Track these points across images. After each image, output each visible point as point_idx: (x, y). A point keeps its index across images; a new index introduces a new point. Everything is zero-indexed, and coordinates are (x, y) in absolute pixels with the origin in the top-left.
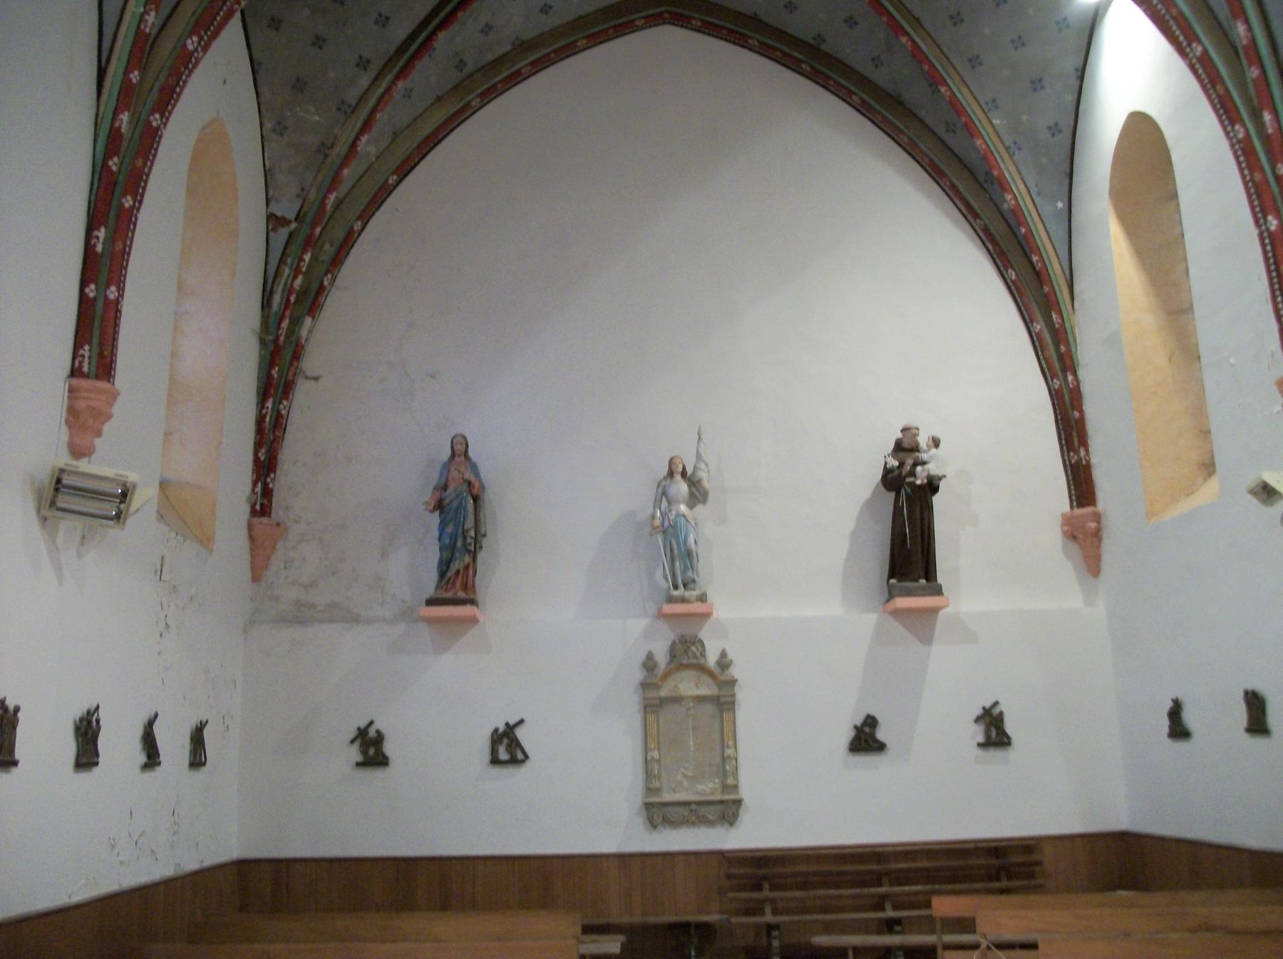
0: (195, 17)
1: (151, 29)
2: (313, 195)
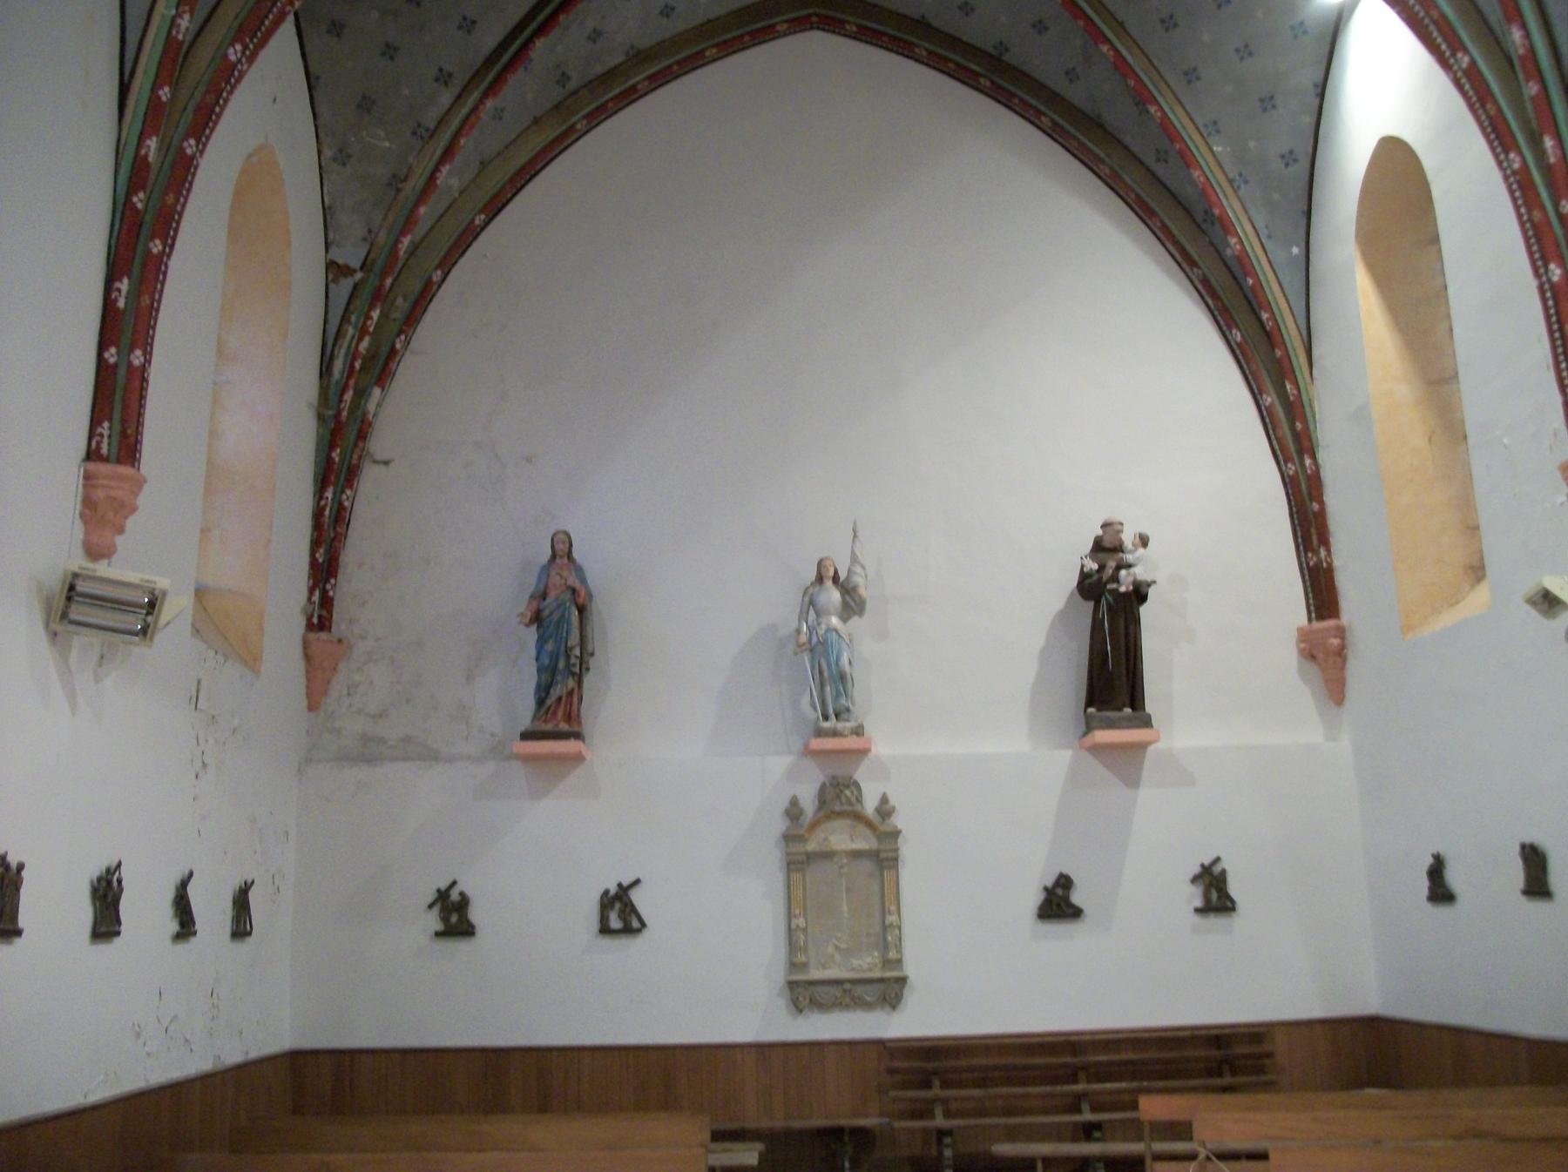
0: (239, 21)
1: (184, 36)
2: (382, 239)
